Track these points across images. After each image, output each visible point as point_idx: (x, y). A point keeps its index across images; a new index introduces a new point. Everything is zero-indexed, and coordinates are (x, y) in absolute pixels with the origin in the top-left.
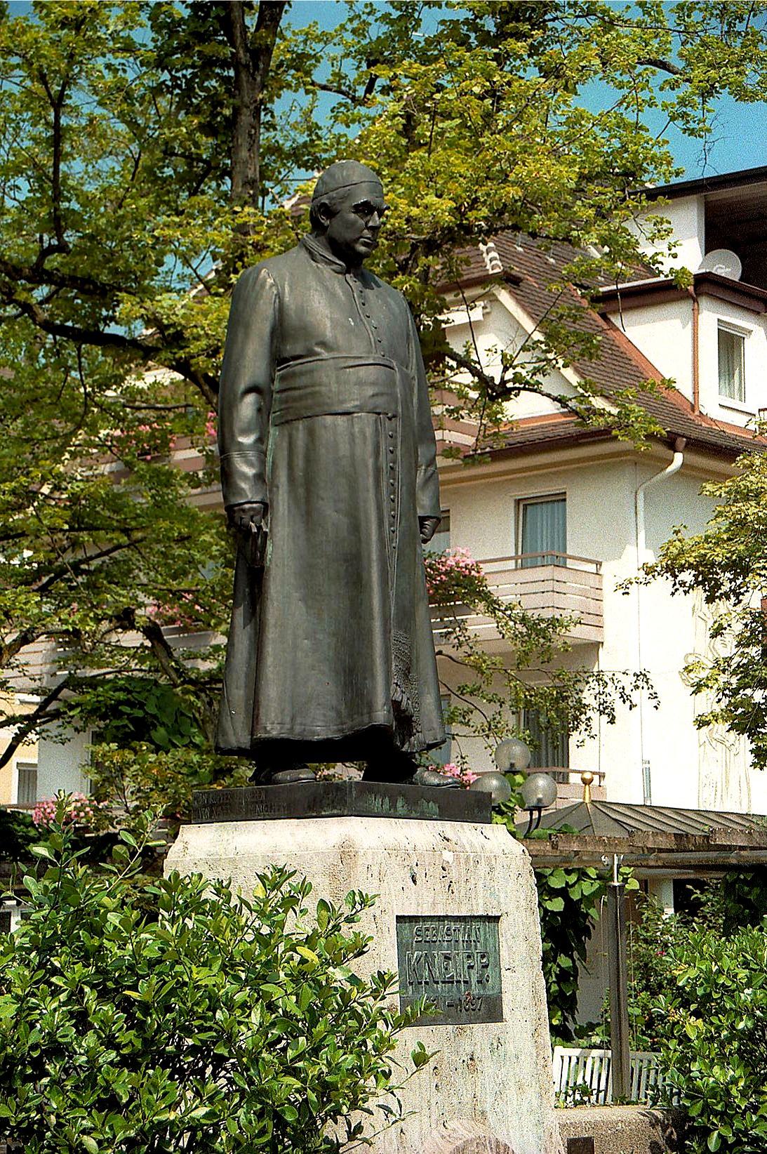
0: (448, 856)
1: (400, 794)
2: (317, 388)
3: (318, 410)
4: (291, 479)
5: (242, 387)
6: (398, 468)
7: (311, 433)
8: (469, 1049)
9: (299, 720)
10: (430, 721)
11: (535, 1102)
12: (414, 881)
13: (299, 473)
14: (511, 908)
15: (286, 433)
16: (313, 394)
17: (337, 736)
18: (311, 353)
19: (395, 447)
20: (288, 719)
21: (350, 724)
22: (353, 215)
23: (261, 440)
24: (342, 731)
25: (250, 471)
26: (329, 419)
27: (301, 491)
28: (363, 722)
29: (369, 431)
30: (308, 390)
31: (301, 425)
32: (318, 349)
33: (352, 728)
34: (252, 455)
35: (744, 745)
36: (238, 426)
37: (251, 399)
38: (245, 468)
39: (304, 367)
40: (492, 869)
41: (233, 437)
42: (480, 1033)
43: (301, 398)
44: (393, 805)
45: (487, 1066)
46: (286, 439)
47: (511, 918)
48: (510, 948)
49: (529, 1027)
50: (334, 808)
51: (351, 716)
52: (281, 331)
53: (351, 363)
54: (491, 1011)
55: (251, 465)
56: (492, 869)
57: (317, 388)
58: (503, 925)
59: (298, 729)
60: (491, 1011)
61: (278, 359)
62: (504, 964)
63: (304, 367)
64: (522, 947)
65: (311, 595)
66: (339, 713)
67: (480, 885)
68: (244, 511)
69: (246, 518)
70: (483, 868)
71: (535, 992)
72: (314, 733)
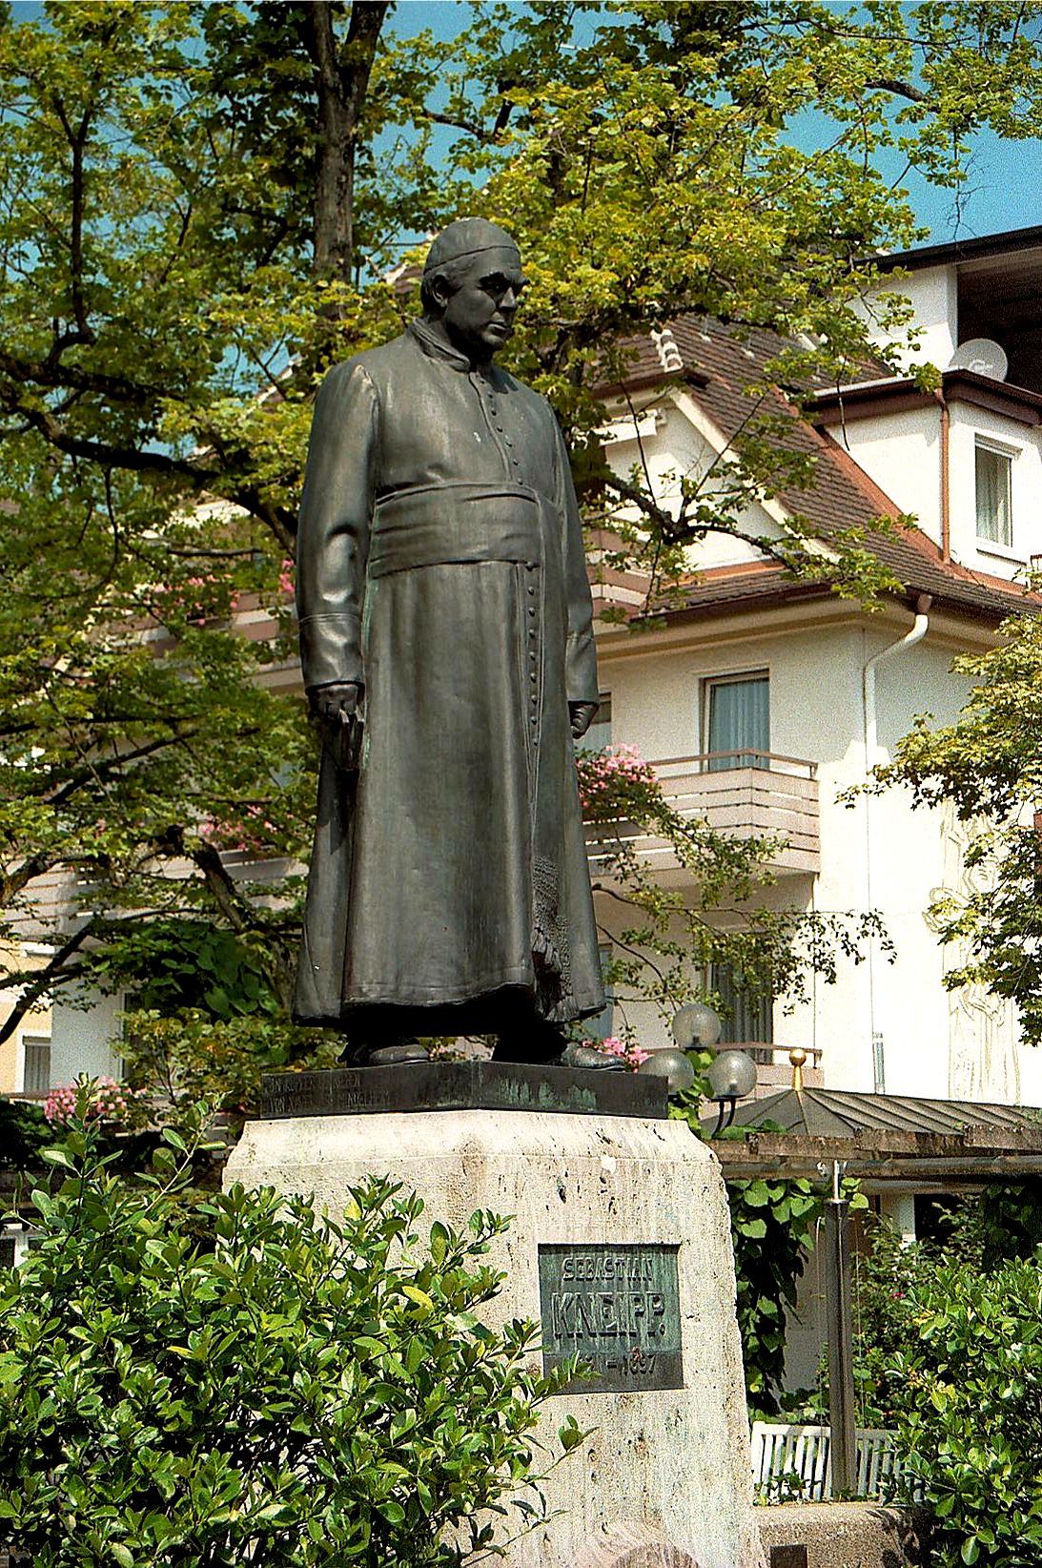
0: (608, 1163)
1: (544, 1078)
2: (431, 528)
3: (432, 557)
4: (396, 651)
5: (329, 525)
6: (541, 636)
7: (422, 588)
8: (637, 1426)
9: (406, 979)
10: (585, 980)
11: (727, 1497)
12: (563, 1198)
13: (406, 643)
14: (694, 1233)
15: (389, 588)
16: (425, 535)
17: (457, 1000)
18: (423, 480)
19: (537, 607)
20: (391, 977)
21: (475, 983)
22: (479, 293)
23: (354, 598)
24: (464, 993)
25: (340, 641)
26: (447, 569)
27: (409, 667)
28: (493, 982)
29: (501, 586)
30: (419, 530)
31: (408, 578)
32: (432, 475)
33: (478, 989)
34: (342, 618)
35: (1011, 1012)
36: (323, 578)
37: (340, 541)
38: (333, 636)
39: (413, 499)
40: (668, 1181)
41: (316, 593)
42: (652, 1404)
43: (409, 541)
44: (534, 1094)
45: (662, 1448)
46: (389, 597)
47: (694, 1247)
48: (693, 1288)
49: (719, 1396)
50: (454, 1097)
51: (476, 973)
52: (381, 449)
53: (477, 493)
54: (667, 1373)
55: (341, 631)
56: (668, 1181)
57: (431, 528)
58: (683, 1257)
59: (404, 990)
60: (667, 1373)
61: (377, 488)
62: (685, 1310)
63: (413, 499)
64: (710, 1287)
65: (422, 809)
66: (460, 969)
67: (652, 1202)
68: (331, 694)
69: (334, 703)
70: (656, 1180)
71: (727, 1348)
72: (426, 996)
